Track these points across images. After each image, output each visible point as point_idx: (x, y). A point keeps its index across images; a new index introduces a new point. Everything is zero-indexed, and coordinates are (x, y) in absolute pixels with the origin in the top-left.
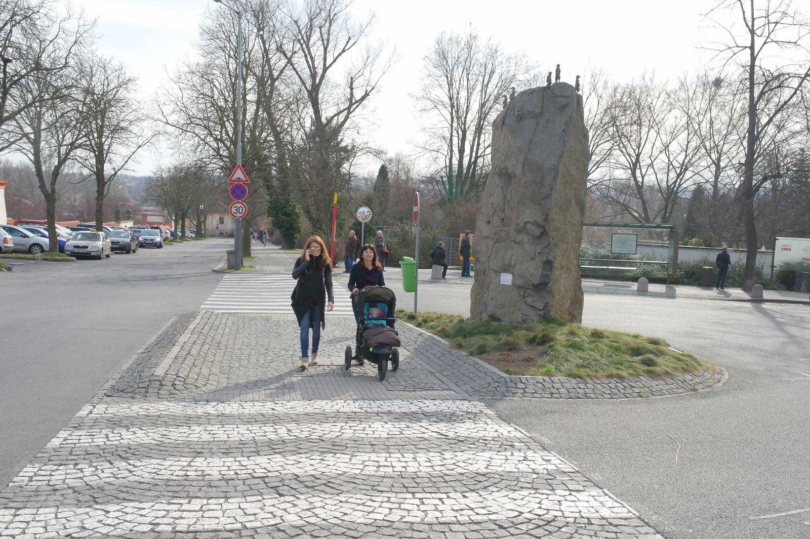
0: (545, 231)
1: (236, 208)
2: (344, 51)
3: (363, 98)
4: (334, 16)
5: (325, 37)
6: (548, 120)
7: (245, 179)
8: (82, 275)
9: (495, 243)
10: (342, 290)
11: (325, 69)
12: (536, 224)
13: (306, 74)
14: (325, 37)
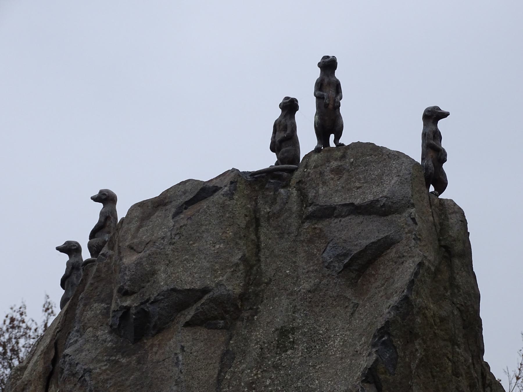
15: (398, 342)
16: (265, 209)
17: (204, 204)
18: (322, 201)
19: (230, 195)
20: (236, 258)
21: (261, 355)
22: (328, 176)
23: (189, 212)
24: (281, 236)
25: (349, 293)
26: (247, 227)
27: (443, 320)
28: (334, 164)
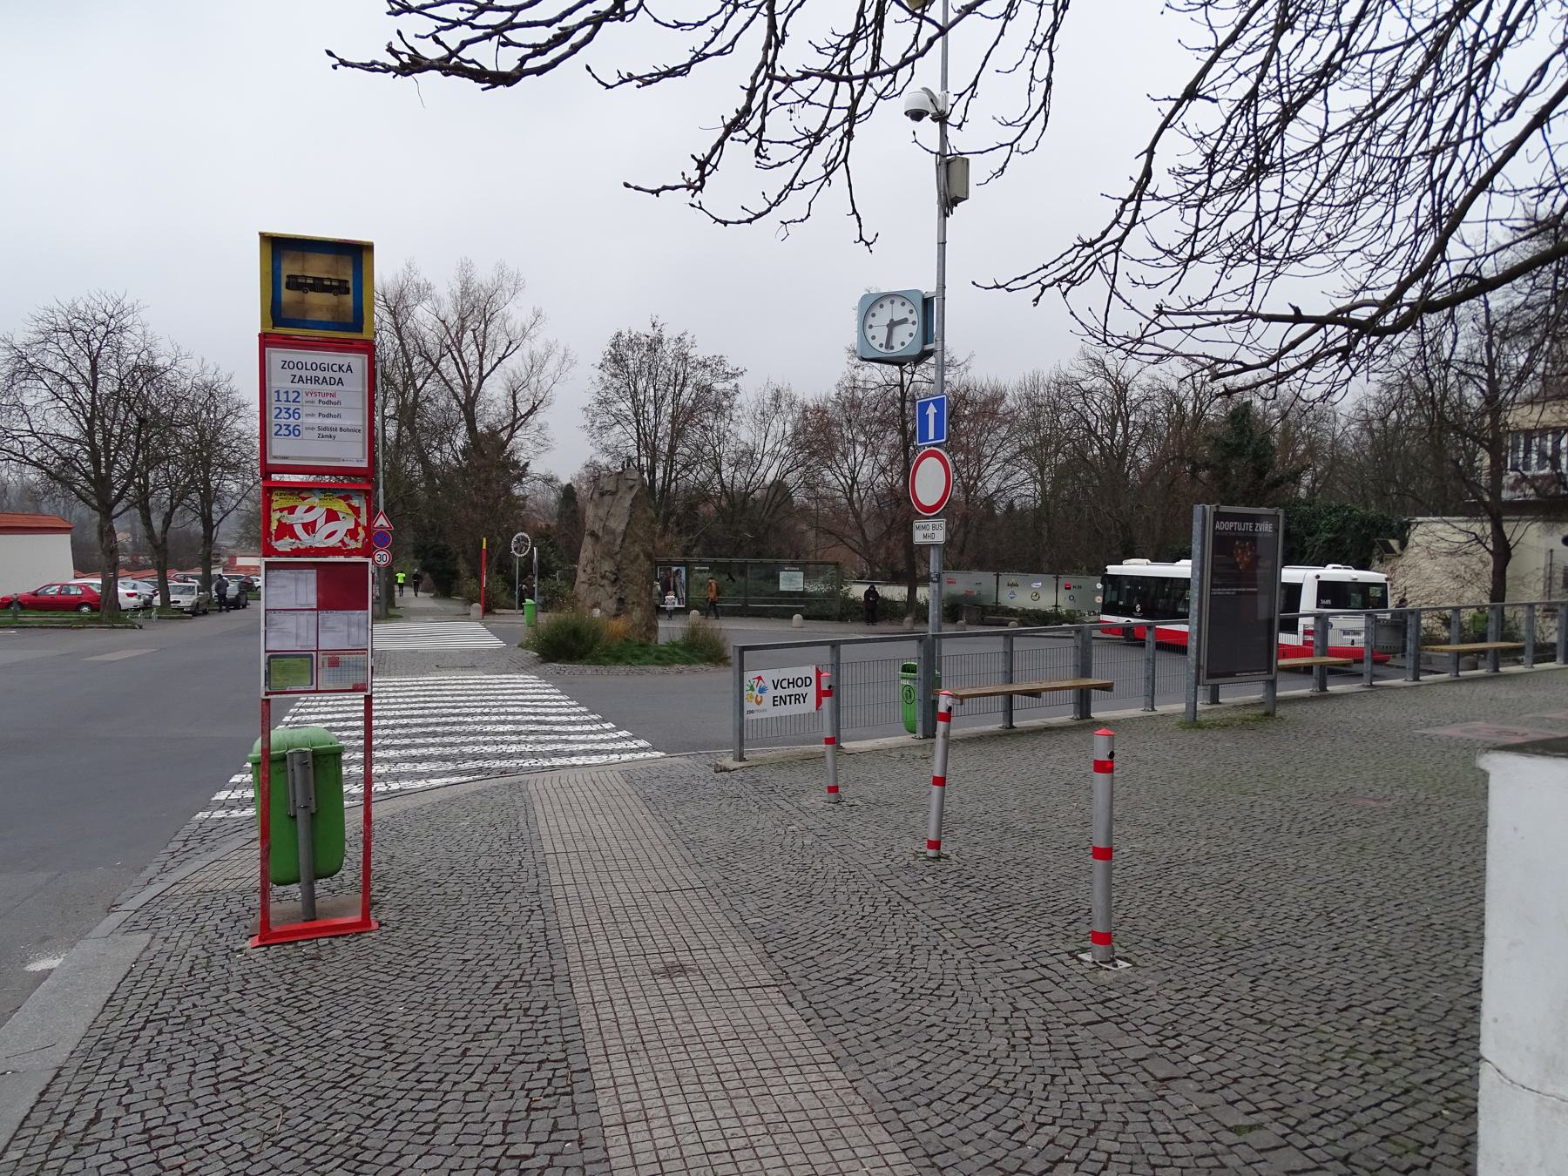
3: (530, 413)
5: (480, 340)
10: (577, 710)
11: (482, 379)
12: (611, 572)
13: (457, 383)
14: (480, 340)
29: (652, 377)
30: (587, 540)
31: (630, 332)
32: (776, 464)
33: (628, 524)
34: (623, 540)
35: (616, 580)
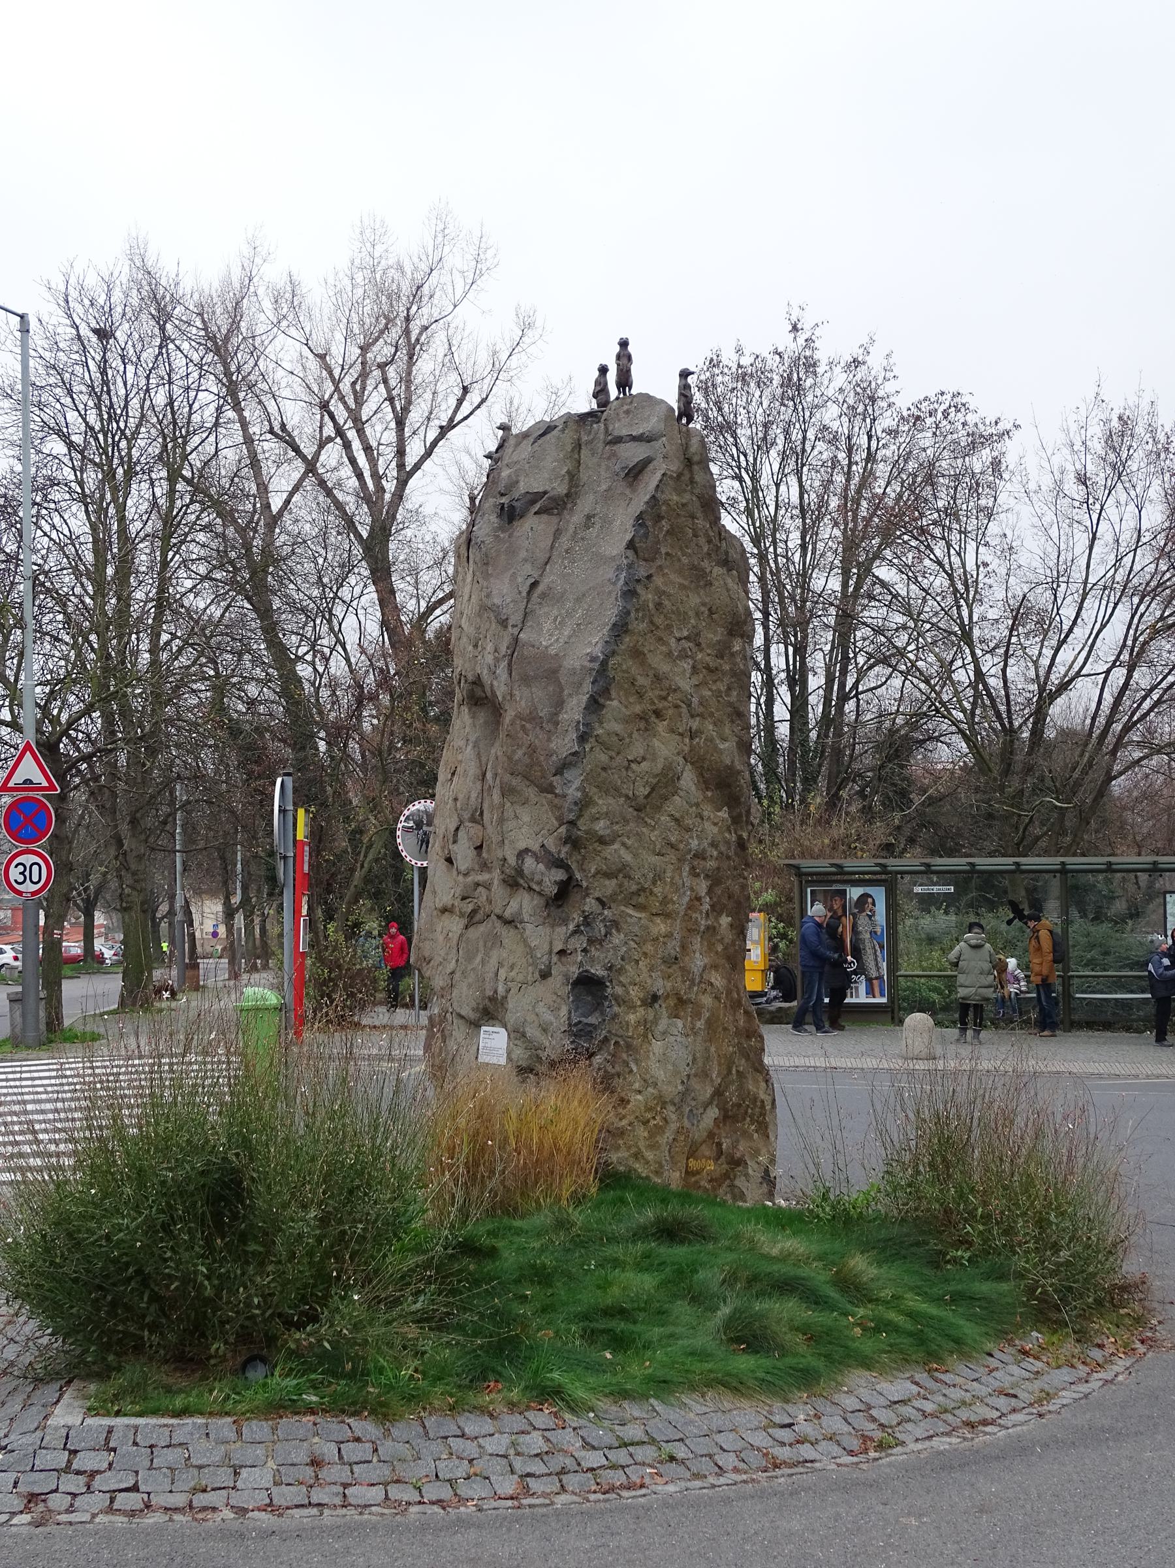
0: (570, 878)
1: (21, 868)
2: (451, 425)
4: (421, 334)
6: (589, 517)
7: (45, 784)
8: (1149, 1069)
9: (467, 927)
11: (404, 477)
15: (649, 523)
16: (585, 438)
17: (548, 436)
18: (616, 433)
19: (563, 430)
20: (563, 472)
21: (575, 533)
22: (622, 415)
23: (540, 442)
24: (593, 455)
25: (628, 492)
26: (573, 450)
27: (683, 505)
28: (626, 407)
29: (796, 456)
30: (464, 723)
31: (739, 351)
32: (1123, 614)
33: (620, 629)
34: (595, 705)
35: (565, 892)
